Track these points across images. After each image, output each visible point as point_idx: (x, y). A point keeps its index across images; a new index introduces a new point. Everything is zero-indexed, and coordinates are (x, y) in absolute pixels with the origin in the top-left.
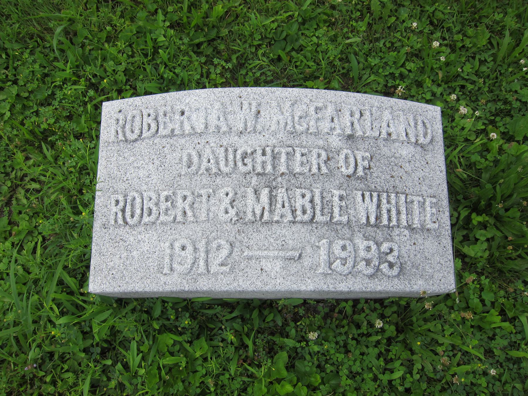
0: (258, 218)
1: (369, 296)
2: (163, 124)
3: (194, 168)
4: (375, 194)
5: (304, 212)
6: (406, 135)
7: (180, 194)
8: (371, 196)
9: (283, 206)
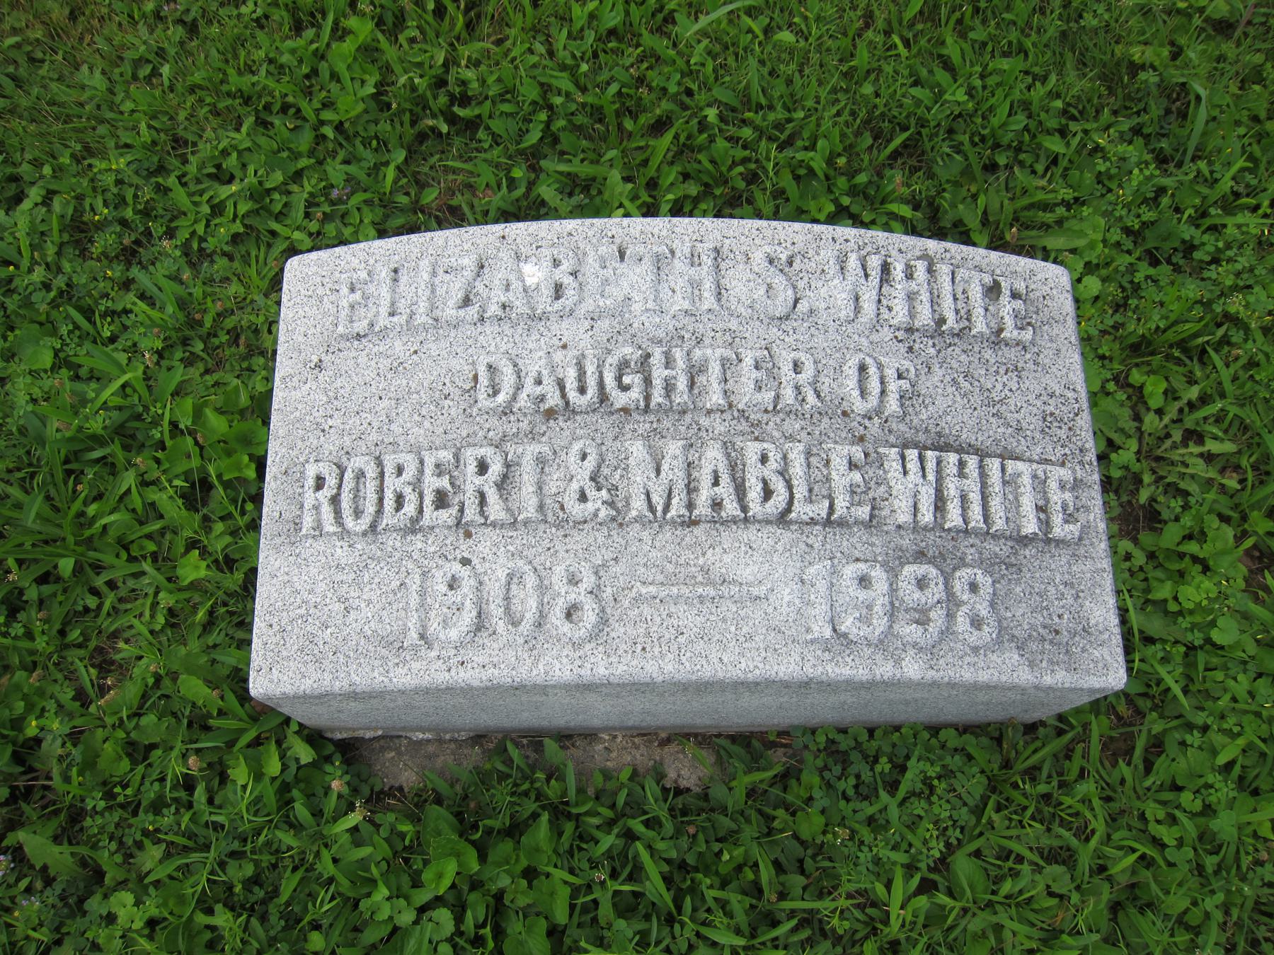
0: (659, 514)
1: (951, 712)
2: (957, 501)
3: (501, 398)
4: (972, 462)
5: (768, 493)
6: (342, 620)
7: (470, 457)
8: (921, 459)
9: (716, 483)
